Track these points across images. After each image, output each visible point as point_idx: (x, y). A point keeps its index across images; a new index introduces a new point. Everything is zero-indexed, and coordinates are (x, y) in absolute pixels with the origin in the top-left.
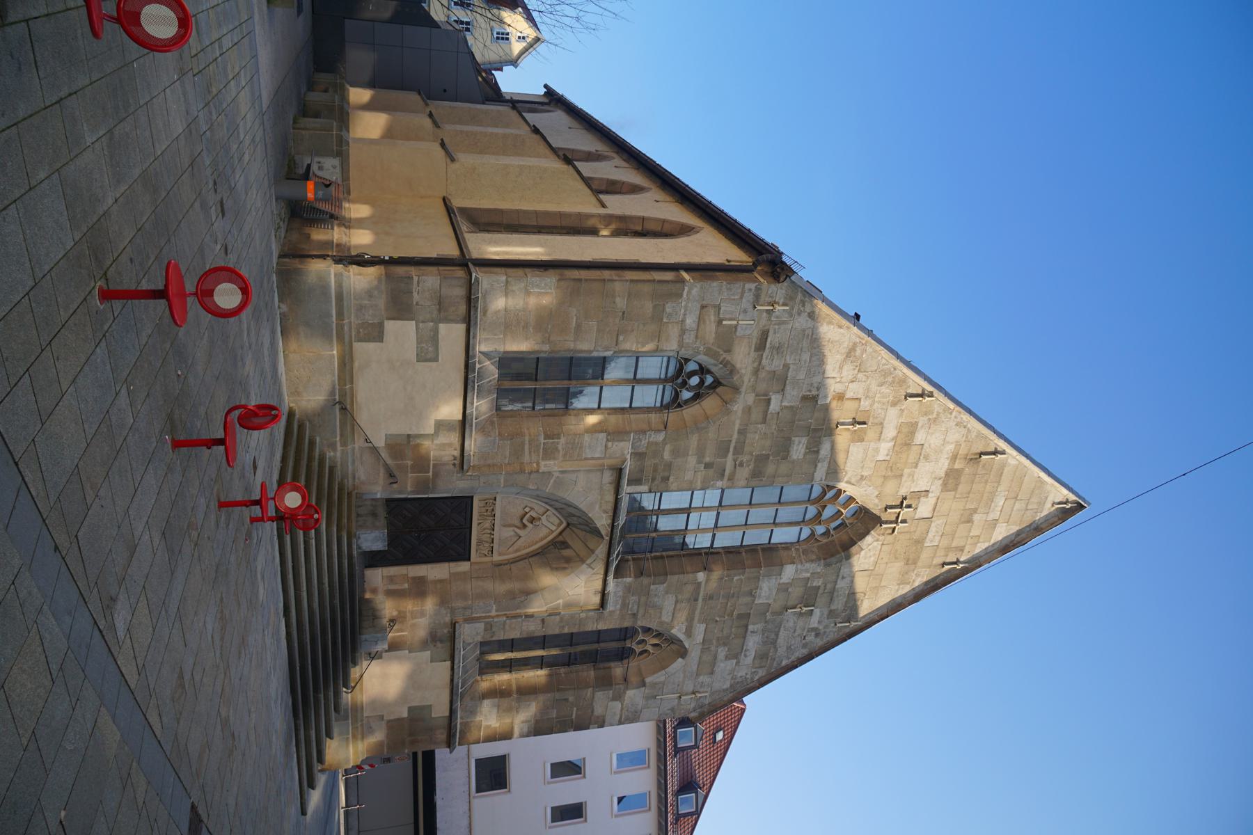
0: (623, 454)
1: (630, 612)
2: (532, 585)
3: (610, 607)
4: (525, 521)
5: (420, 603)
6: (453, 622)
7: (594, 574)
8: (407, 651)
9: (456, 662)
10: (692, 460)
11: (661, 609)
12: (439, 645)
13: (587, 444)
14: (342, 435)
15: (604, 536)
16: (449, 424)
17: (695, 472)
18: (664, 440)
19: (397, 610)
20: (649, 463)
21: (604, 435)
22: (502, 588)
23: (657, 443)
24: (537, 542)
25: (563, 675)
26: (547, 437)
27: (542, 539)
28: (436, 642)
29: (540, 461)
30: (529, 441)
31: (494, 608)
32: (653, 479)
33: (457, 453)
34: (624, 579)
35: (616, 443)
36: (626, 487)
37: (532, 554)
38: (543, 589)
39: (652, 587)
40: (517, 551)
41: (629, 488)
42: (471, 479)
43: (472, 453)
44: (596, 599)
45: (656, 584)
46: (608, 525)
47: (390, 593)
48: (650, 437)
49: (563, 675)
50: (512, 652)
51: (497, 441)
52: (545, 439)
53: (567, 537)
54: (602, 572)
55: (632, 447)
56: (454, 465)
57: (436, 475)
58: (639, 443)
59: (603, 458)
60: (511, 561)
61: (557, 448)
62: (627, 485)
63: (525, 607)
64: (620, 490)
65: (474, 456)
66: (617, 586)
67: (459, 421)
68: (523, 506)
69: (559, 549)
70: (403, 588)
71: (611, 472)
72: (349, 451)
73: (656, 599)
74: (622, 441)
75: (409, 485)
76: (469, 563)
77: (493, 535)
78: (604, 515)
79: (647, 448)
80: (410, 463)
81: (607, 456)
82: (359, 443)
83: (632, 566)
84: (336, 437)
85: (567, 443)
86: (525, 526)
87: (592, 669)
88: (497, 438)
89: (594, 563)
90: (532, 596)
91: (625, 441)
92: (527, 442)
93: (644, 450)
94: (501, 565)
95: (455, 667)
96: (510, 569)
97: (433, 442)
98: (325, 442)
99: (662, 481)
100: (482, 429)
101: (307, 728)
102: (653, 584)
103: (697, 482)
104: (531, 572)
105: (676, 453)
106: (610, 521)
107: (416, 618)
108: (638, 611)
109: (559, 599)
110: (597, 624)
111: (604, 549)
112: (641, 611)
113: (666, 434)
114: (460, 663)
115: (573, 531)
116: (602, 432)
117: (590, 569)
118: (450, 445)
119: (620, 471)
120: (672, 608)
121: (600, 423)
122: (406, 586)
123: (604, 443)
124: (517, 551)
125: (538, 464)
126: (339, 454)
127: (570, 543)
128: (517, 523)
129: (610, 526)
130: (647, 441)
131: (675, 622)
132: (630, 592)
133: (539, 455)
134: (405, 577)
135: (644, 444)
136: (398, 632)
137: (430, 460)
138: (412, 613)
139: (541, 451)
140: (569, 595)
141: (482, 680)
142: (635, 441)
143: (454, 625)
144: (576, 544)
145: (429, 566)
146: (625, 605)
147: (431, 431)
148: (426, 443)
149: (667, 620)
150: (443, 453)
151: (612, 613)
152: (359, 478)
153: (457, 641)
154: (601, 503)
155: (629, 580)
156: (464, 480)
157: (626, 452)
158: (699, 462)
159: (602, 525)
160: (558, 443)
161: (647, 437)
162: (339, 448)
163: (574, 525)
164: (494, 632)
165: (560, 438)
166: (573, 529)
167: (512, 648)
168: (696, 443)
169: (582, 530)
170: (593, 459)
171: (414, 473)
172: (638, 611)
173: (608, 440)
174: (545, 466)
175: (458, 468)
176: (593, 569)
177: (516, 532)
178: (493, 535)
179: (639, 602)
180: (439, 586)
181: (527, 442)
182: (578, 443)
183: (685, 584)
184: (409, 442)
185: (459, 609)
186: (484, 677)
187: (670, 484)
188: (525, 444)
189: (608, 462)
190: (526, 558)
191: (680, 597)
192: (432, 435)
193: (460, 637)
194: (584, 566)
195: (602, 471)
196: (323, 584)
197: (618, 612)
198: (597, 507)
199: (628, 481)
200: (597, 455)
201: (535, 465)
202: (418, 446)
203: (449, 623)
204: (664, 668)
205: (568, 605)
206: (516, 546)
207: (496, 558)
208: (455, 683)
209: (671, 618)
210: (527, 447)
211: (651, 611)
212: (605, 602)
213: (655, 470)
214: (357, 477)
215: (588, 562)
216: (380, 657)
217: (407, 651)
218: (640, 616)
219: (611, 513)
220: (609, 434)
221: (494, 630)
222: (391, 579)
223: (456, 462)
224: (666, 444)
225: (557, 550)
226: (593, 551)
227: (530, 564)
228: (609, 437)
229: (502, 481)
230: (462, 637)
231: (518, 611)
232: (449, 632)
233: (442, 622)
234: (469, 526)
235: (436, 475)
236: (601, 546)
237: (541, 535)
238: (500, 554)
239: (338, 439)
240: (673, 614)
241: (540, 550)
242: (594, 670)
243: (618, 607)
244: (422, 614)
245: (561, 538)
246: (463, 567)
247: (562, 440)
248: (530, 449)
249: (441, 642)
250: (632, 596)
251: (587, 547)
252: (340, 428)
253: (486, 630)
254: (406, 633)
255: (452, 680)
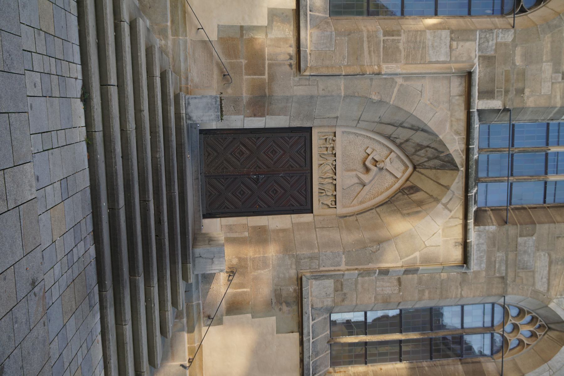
0: (471, 58)
1: (497, 275)
2: (383, 233)
3: (474, 265)
4: (368, 163)
5: (261, 250)
6: (300, 276)
7: (452, 217)
8: (249, 315)
9: (305, 331)
10: (547, 68)
11: (533, 272)
12: (285, 308)
13: (430, 43)
14: (173, 22)
15: (459, 166)
16: (283, 13)
17: (553, 83)
18: (514, 40)
19: (237, 257)
20: (500, 70)
21: (447, 32)
22: (350, 238)
23: (506, 45)
24: (382, 193)
25: (426, 368)
26: (386, 33)
27: (387, 189)
28: (281, 304)
29: (381, 64)
30: (368, 38)
31: (344, 259)
32: (507, 92)
33: (292, 51)
34: (487, 227)
35: (461, 43)
36: (477, 101)
37: (377, 205)
38: (396, 236)
39: (520, 240)
40: (361, 203)
41: (481, 102)
42: (309, 85)
43: (308, 51)
44: (457, 254)
45: (524, 236)
46: (462, 151)
47: (230, 240)
48: (497, 36)
49: (426, 368)
50: (366, 334)
51: (334, 37)
52: (384, 36)
53: (416, 181)
54: (461, 215)
55: (479, 50)
56: (290, 65)
57: (272, 78)
58: (486, 44)
59: (449, 62)
60: (356, 213)
61: (398, 47)
62: (478, 99)
63: (378, 261)
64: (472, 100)
65: (310, 54)
66: (479, 236)
67: (293, 10)
68: (364, 147)
69: (407, 195)
70: (243, 236)
71: (459, 80)
72: (181, 42)
73: (526, 258)
74: (468, 40)
75: (244, 90)
76: (312, 214)
77: (335, 180)
78: (457, 138)
79: (496, 50)
80: (244, 62)
81: (453, 59)
82: (191, 35)
83: (492, 216)
84: (167, 22)
85: (409, 42)
86: (367, 170)
87: (459, 363)
88: (334, 33)
89: (451, 202)
90: (385, 245)
91: (471, 40)
92: (365, 39)
93: (492, 53)
94: (346, 216)
95: (304, 339)
96: (357, 220)
97: (267, 35)
98: (155, 27)
99: (516, 94)
100: (317, 24)
101: (119, 322)
102: (521, 236)
103: (555, 96)
104: (380, 221)
105: (528, 57)
106: (463, 146)
107: (258, 269)
108: (507, 274)
109: (414, 251)
110: (462, 290)
111: (460, 183)
112: (511, 275)
113: (515, 33)
114: (309, 339)
115: (422, 174)
116: (445, 29)
117: (446, 212)
118: (285, 40)
119: (469, 75)
120: (546, 272)
121: (440, 23)
122: (246, 234)
123: (448, 44)
124: (361, 203)
125: (379, 66)
126: (170, 43)
127: (419, 185)
128: (360, 167)
129: (465, 152)
130: (495, 42)
131: (553, 292)
132: (494, 246)
133: (379, 56)
134: (245, 226)
135: (492, 46)
136: (240, 288)
137: (264, 60)
138: (253, 260)
139: (381, 50)
140: (426, 247)
141: (335, 372)
142: (482, 41)
143: (300, 280)
144: (427, 185)
145: (270, 217)
146: (490, 264)
147: (263, 21)
148: (260, 37)
149: (542, 289)
150: (278, 50)
151: (476, 273)
152: (192, 81)
153: (305, 300)
154: (452, 121)
155: (492, 228)
156: (301, 85)
157: (473, 55)
158: (556, 71)
159: (455, 151)
160: (399, 41)
161: (495, 36)
162: (170, 37)
163: (421, 165)
164: (345, 294)
165: (400, 35)
166: (422, 171)
167: (366, 329)
168: (549, 45)
169: (431, 168)
170: (437, 62)
171: (250, 75)
172: (507, 274)
173: (452, 39)
174: (387, 68)
175: (294, 70)
176: (451, 211)
177: (359, 178)
178: (335, 180)
179: (507, 261)
180: (281, 235)
181: (365, 39)
182: (420, 42)
183: (558, 237)
184: (242, 35)
185: (304, 258)
186: (337, 369)
187: (525, 98)
188: (363, 41)
189: (454, 66)
190: (372, 209)
191: (554, 256)
192: (266, 27)
193: (308, 298)
194: (440, 206)
195: (449, 79)
196: (141, 111)
197: (484, 274)
198: (448, 125)
199: (479, 93)
200: (442, 58)
201: (376, 67)
202: (251, 40)
203: (295, 277)
204: (545, 361)
205: (426, 260)
206: (360, 198)
207: (341, 210)
208: (305, 363)
209: (546, 286)
210: (366, 45)
211: (522, 274)
212: (469, 255)
213: (507, 80)
214: (190, 78)
215: (444, 200)
216: (220, 322)
217: (249, 315)
218: (509, 280)
219: (464, 135)
220: (452, 32)
221: (345, 291)
222: (230, 228)
223: (292, 61)
224: (516, 46)
225: (406, 196)
226: (447, 188)
227: (378, 214)
228: (453, 35)
229: (342, 88)
230: (310, 298)
231: (371, 266)
232: (295, 290)
233: (287, 276)
234: (310, 208)
235: (272, 78)
236: (456, 180)
237: (387, 185)
238: (344, 207)
239: (169, 24)
240: (549, 280)
241: (387, 200)
242: (461, 364)
243: (484, 265)
244: (264, 263)
245: (408, 184)
246: (306, 218)
247: (403, 38)
248: (369, 47)
249: (288, 304)
250: (498, 251)
251: (440, 184)
252: (171, 12)
253: (336, 290)
254: (248, 290)
255: (302, 360)
